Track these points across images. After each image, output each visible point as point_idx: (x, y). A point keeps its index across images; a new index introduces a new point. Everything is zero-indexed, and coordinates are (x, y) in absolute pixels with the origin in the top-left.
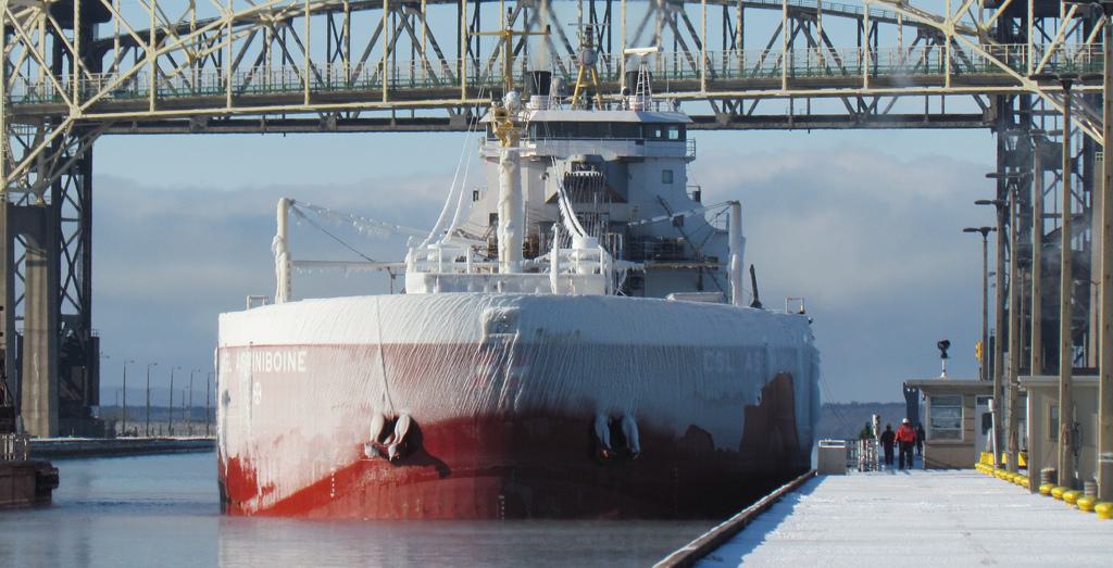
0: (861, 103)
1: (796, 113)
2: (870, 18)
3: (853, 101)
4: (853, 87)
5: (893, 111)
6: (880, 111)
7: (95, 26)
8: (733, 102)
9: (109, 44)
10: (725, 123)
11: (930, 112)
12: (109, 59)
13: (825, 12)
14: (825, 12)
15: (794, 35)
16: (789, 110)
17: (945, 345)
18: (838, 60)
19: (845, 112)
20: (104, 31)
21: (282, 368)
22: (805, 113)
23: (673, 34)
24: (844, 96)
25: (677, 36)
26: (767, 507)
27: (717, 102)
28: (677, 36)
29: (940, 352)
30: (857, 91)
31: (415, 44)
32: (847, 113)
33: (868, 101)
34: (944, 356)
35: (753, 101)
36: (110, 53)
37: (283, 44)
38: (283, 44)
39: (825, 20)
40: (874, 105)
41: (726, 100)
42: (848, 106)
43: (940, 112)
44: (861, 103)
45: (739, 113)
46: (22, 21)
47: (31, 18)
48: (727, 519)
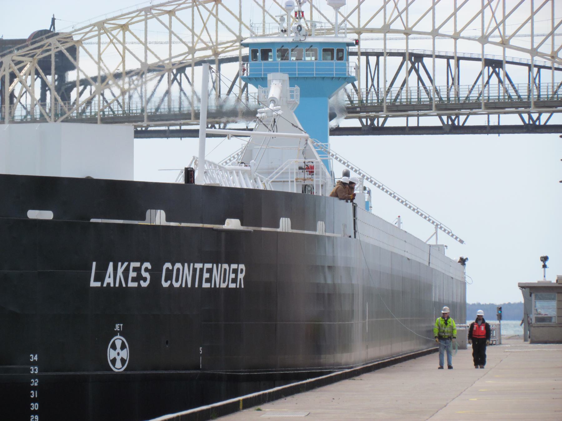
0: (530, 118)
1: (491, 124)
2: (535, 66)
3: (526, 116)
4: (525, 108)
5: (467, 124)
6: (542, 123)
7: (66, 74)
8: (453, 117)
9: (73, 85)
10: (448, 131)
11: (409, 125)
12: (74, 94)
13: (508, 62)
14: (508, 62)
15: (489, 77)
16: (487, 122)
17: (545, 259)
18: (516, 91)
19: (521, 123)
20: (71, 76)
21: (181, 285)
22: (496, 124)
23: (417, 77)
24: (520, 113)
25: (419, 78)
26: (367, 364)
27: (523, 115)
28: (419, 78)
29: (542, 263)
30: (527, 110)
31: (500, 81)
32: (522, 124)
33: (535, 116)
34: (545, 266)
35: (465, 116)
36: (75, 90)
37: (180, 84)
38: (180, 84)
39: (508, 68)
40: (538, 118)
41: (449, 117)
42: (362, 122)
43: (416, 125)
44: (530, 118)
45: (376, 125)
46: (20, 70)
47: (26, 69)
48: (191, 373)
